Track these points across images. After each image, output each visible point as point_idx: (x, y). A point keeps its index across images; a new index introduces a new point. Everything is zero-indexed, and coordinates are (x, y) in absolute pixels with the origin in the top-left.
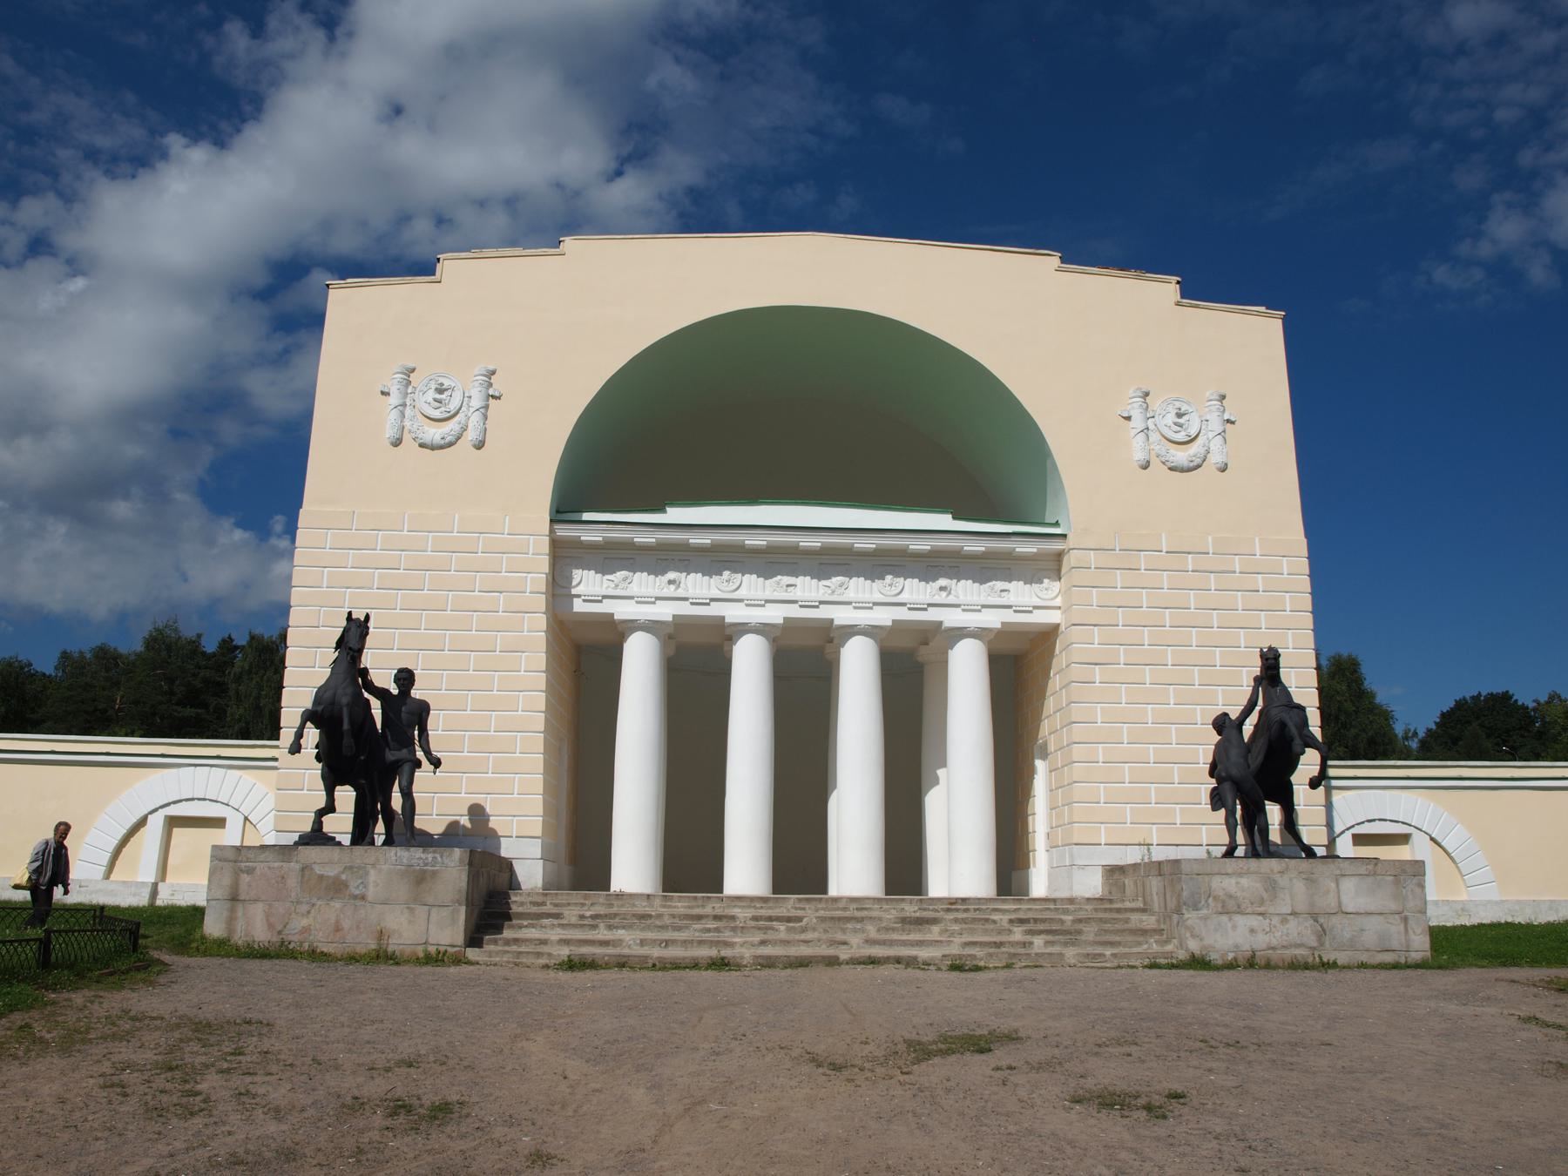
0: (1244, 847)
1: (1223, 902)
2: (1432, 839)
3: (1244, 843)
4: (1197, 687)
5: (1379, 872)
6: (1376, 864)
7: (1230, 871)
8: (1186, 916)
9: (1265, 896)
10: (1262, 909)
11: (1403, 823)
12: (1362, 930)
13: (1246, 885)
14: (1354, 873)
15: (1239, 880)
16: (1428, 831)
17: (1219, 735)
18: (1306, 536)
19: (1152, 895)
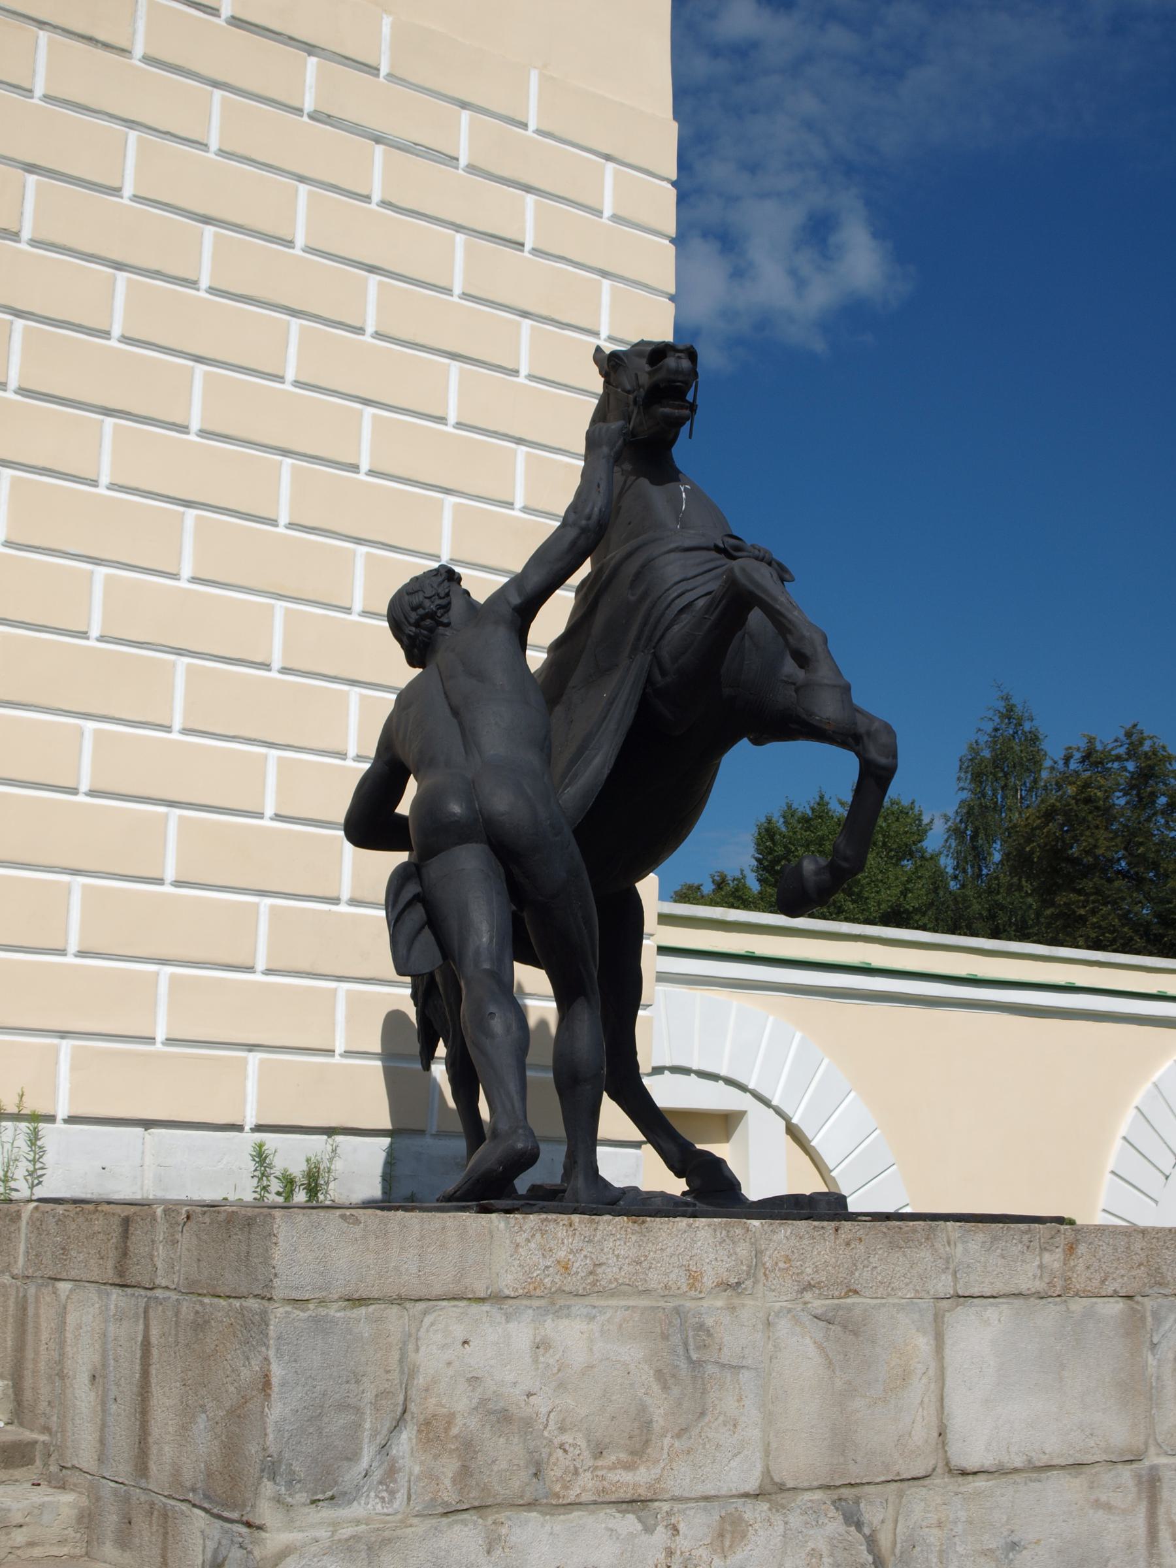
0: (386, 1141)
1: (468, 1448)
2: (793, 1132)
3: (388, 1125)
4: (281, 530)
5: (1079, 1283)
6: (1071, 1249)
7: (508, 1282)
8: (276, 1538)
9: (659, 1409)
10: (639, 1479)
11: (729, 1082)
12: (1014, 1546)
13: (578, 1358)
14: (1000, 1287)
15: (550, 1326)
16: (788, 1111)
17: (413, 662)
18: (677, 115)
19: (60, 1374)
